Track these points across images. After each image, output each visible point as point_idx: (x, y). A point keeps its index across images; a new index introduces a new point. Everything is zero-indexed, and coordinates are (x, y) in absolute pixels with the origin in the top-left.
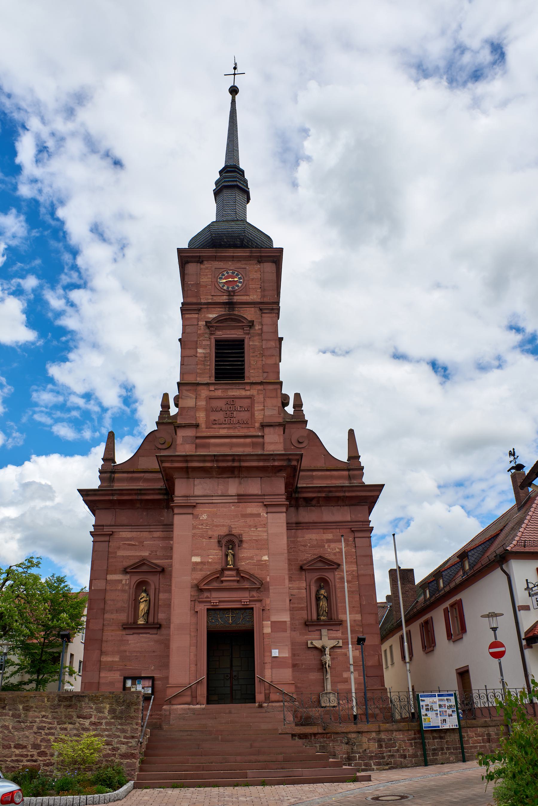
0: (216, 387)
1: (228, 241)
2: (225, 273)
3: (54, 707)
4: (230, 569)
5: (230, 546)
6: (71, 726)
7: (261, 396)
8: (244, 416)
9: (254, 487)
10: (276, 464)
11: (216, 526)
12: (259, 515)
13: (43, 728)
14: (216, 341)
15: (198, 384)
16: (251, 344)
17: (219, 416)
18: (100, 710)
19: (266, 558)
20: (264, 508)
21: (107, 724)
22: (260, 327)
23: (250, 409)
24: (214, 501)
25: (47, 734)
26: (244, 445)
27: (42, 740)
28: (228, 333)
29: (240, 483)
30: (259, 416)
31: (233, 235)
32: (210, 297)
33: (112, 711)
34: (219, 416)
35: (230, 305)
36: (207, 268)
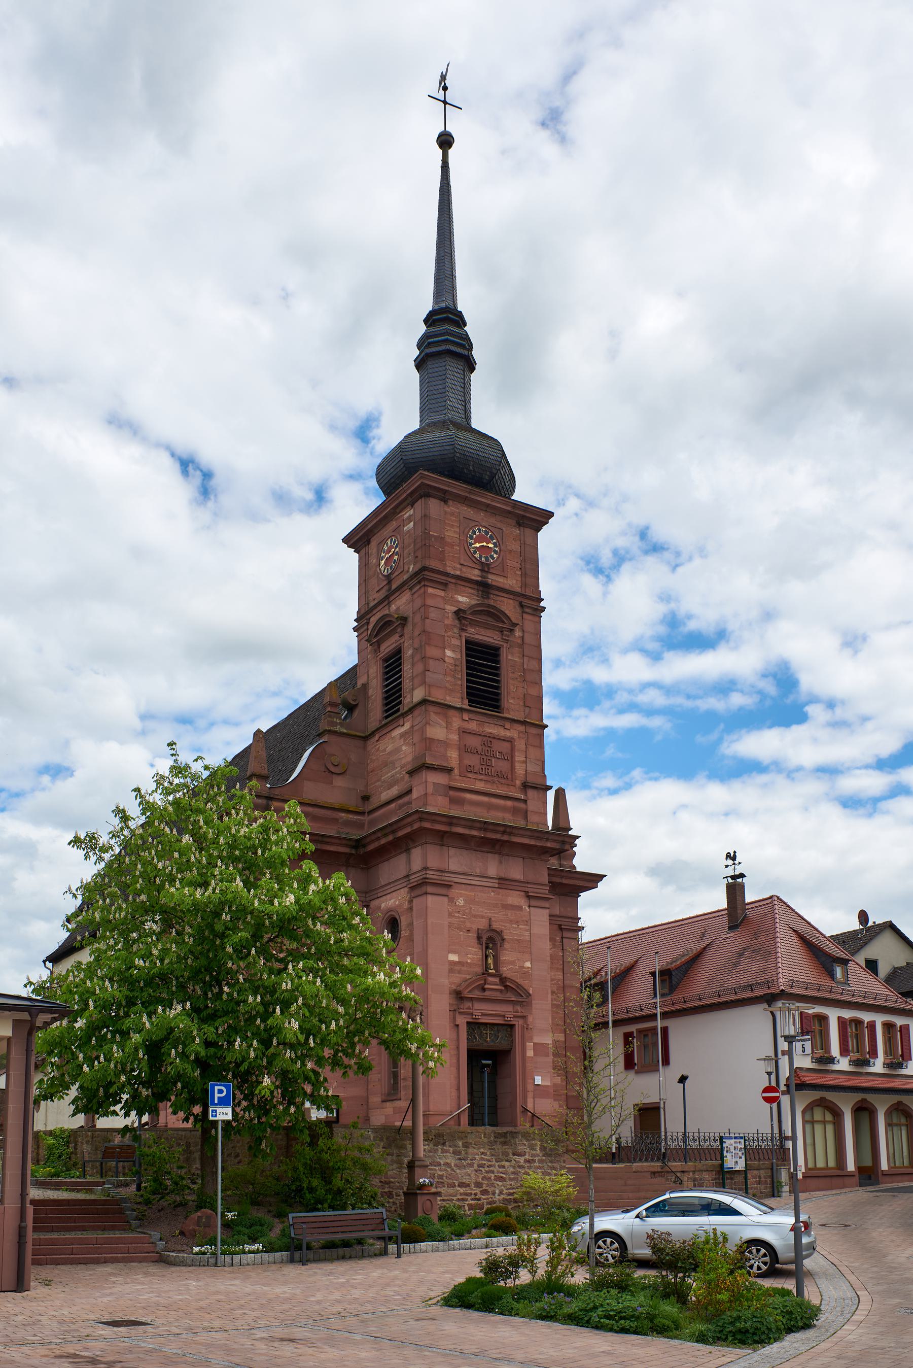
0: (471, 716)
1: (474, 471)
2: (476, 530)
3: (491, 1144)
4: (492, 975)
5: (491, 945)
6: (507, 1164)
7: (523, 742)
8: (503, 766)
9: (516, 870)
10: (549, 845)
11: (475, 916)
12: (520, 908)
13: (482, 1166)
14: (467, 642)
15: (450, 707)
16: (510, 658)
17: (473, 760)
18: (532, 1148)
19: (528, 964)
20: (526, 900)
21: (540, 1161)
22: (521, 634)
23: (510, 758)
24: (473, 882)
25: (487, 1172)
26: (504, 809)
27: (484, 1178)
28: (483, 633)
29: (501, 862)
30: (520, 770)
31: (484, 463)
32: (459, 566)
33: (543, 1148)
34: (473, 760)
35: (484, 587)
36: (452, 514)
